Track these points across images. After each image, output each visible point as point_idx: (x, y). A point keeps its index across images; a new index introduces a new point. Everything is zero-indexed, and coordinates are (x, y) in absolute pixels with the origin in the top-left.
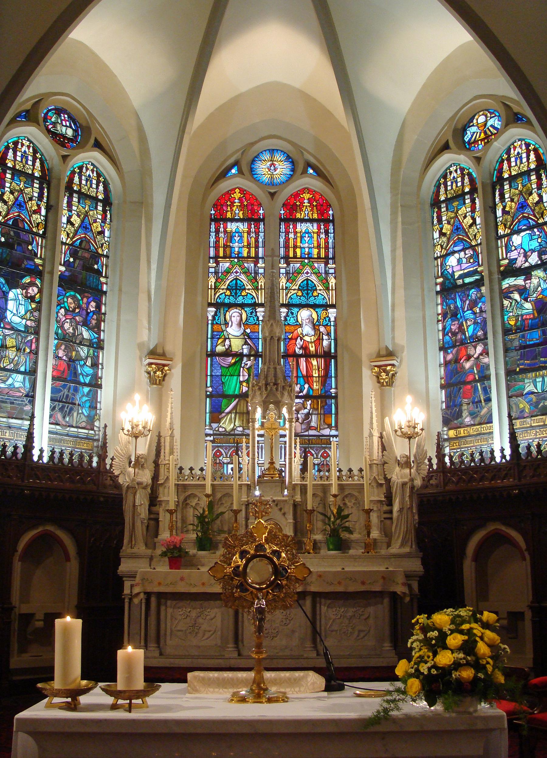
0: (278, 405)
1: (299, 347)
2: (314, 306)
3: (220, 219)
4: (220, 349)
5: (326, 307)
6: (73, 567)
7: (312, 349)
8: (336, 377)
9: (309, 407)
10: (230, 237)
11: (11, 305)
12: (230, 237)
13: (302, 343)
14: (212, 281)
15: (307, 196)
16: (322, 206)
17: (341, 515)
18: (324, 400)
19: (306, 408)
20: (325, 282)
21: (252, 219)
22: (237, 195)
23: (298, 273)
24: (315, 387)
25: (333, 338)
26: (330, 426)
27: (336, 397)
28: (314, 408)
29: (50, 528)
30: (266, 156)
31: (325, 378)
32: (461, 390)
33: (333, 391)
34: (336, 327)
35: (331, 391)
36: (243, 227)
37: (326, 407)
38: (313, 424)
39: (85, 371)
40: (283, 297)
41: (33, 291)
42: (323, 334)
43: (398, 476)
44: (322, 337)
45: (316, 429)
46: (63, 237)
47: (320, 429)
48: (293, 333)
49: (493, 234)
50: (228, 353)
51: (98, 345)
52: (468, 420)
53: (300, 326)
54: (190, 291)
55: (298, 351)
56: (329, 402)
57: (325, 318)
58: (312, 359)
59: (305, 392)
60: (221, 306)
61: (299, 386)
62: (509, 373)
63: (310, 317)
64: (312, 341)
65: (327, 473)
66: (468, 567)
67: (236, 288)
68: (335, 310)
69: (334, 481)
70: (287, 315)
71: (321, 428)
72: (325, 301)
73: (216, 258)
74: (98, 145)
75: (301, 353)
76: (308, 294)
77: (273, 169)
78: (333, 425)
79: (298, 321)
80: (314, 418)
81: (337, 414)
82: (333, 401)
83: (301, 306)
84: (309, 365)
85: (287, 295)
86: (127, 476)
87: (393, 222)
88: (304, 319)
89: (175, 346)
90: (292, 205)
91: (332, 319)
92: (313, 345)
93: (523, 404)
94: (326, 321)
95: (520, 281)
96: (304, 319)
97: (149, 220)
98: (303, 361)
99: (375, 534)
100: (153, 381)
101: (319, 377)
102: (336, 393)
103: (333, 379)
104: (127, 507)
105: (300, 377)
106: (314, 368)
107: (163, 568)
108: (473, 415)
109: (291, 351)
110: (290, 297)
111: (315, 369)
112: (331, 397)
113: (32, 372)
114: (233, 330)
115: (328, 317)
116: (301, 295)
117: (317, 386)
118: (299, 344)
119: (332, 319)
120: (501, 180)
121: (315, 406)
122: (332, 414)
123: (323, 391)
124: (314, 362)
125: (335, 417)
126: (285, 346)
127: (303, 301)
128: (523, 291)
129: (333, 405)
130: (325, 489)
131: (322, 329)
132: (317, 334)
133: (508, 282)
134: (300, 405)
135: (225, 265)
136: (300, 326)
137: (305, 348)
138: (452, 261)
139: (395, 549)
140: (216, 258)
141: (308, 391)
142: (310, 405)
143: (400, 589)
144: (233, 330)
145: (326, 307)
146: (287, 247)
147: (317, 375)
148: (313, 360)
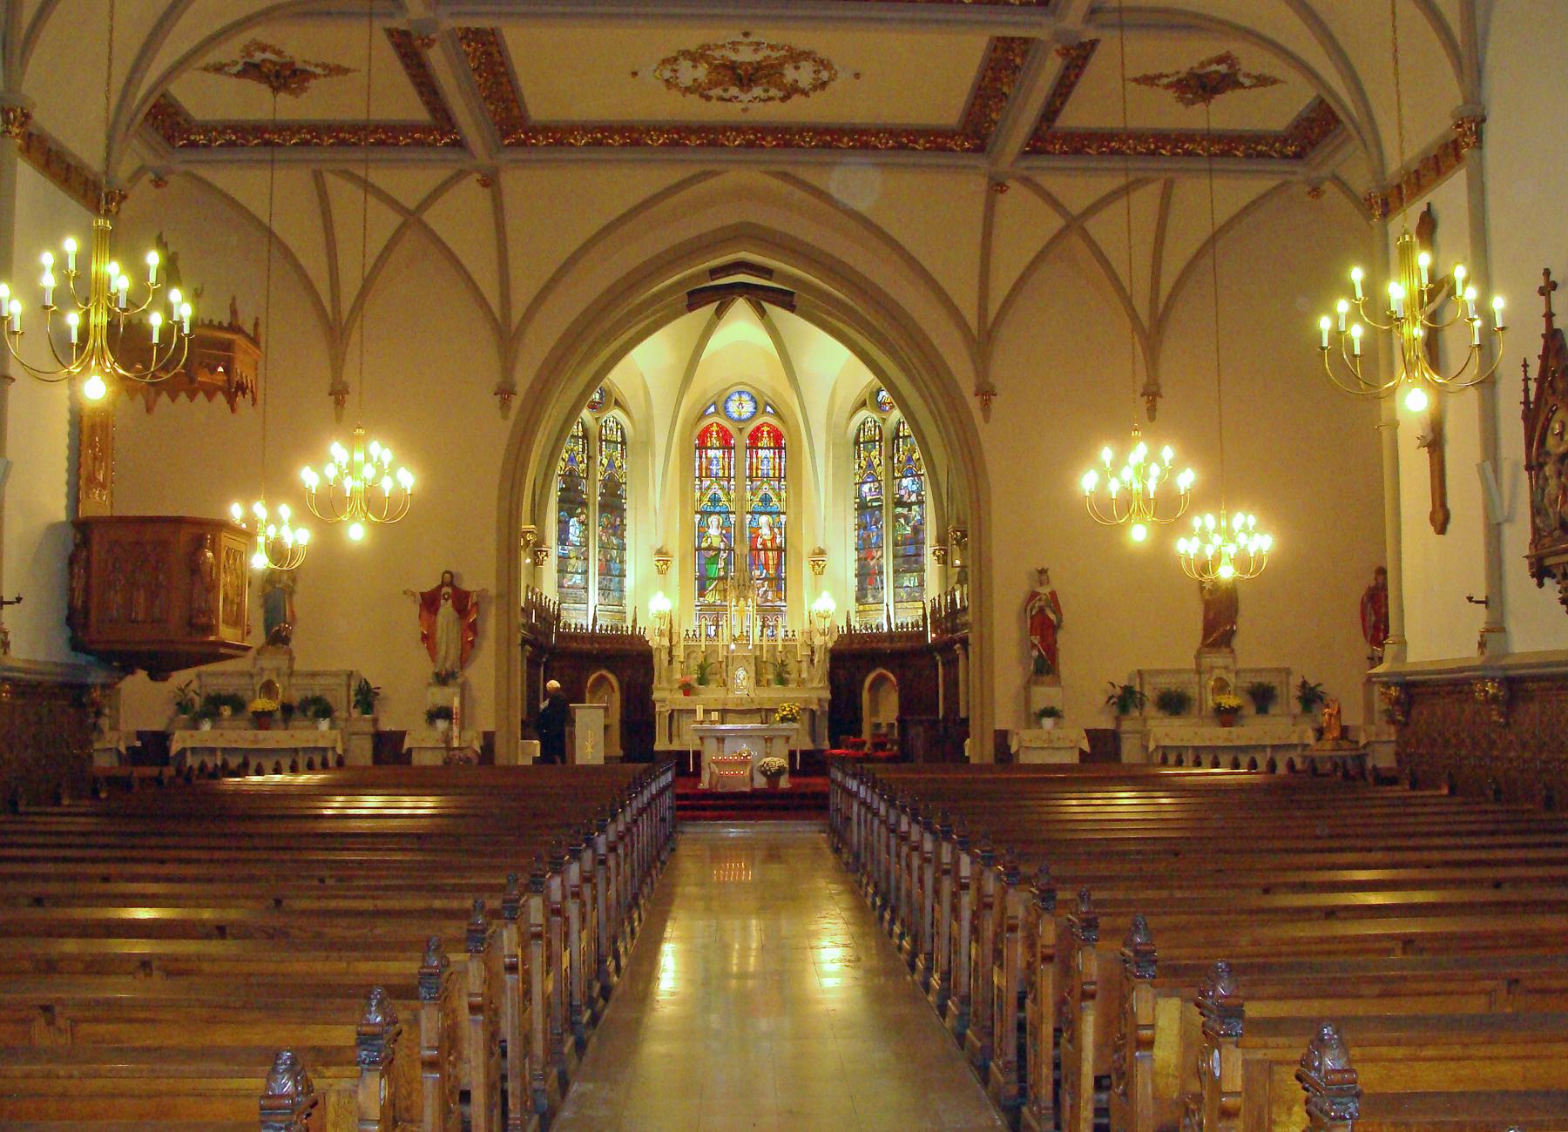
0: (746, 599)
2: (770, 513)
3: (702, 446)
4: (704, 545)
5: (779, 513)
6: (617, 696)
10: (710, 462)
11: (572, 530)
12: (710, 462)
14: (698, 494)
15: (766, 429)
16: (777, 436)
17: (783, 664)
18: (778, 582)
20: (779, 495)
21: (726, 445)
22: (715, 428)
23: (758, 488)
29: (604, 672)
30: (736, 397)
31: (778, 565)
32: (867, 577)
36: (719, 453)
39: (615, 567)
41: (583, 517)
43: (818, 641)
46: (599, 477)
50: (710, 548)
51: (622, 548)
52: (871, 600)
54: (683, 505)
60: (705, 514)
62: (896, 572)
65: (1018, 61)
66: (866, 696)
67: (715, 500)
69: (780, 643)
73: (700, 478)
74: (617, 403)
77: (741, 408)
83: (761, 513)
86: (654, 641)
87: (827, 457)
89: (674, 547)
90: (755, 437)
93: (903, 593)
95: (905, 511)
97: (653, 455)
99: (804, 675)
100: (660, 572)
104: (656, 660)
107: (680, 695)
108: (874, 597)
113: (586, 572)
114: (713, 531)
120: (897, 437)
128: (907, 518)
130: (775, 647)
133: (899, 510)
135: (706, 483)
137: (764, 544)
138: (866, 488)
139: (815, 684)
140: (700, 478)
143: (815, 707)
144: (713, 531)
145: (779, 513)
146: (751, 468)
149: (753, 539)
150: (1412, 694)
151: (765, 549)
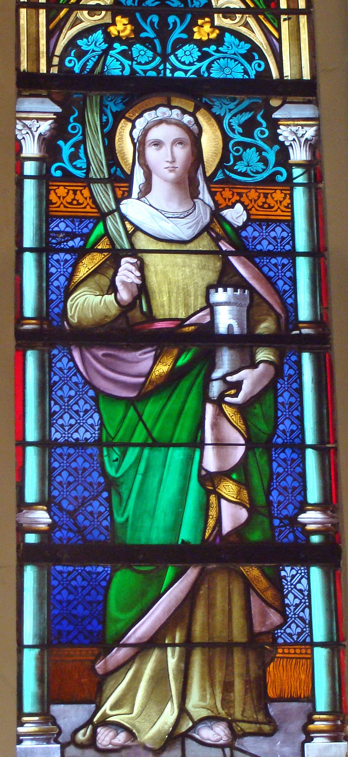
2: (199, 92)
33: (311, 518)
35: (304, 518)
83: (138, 92)
85: (53, 34)
91: (299, 154)
119: (299, 154)
127: (144, 61)
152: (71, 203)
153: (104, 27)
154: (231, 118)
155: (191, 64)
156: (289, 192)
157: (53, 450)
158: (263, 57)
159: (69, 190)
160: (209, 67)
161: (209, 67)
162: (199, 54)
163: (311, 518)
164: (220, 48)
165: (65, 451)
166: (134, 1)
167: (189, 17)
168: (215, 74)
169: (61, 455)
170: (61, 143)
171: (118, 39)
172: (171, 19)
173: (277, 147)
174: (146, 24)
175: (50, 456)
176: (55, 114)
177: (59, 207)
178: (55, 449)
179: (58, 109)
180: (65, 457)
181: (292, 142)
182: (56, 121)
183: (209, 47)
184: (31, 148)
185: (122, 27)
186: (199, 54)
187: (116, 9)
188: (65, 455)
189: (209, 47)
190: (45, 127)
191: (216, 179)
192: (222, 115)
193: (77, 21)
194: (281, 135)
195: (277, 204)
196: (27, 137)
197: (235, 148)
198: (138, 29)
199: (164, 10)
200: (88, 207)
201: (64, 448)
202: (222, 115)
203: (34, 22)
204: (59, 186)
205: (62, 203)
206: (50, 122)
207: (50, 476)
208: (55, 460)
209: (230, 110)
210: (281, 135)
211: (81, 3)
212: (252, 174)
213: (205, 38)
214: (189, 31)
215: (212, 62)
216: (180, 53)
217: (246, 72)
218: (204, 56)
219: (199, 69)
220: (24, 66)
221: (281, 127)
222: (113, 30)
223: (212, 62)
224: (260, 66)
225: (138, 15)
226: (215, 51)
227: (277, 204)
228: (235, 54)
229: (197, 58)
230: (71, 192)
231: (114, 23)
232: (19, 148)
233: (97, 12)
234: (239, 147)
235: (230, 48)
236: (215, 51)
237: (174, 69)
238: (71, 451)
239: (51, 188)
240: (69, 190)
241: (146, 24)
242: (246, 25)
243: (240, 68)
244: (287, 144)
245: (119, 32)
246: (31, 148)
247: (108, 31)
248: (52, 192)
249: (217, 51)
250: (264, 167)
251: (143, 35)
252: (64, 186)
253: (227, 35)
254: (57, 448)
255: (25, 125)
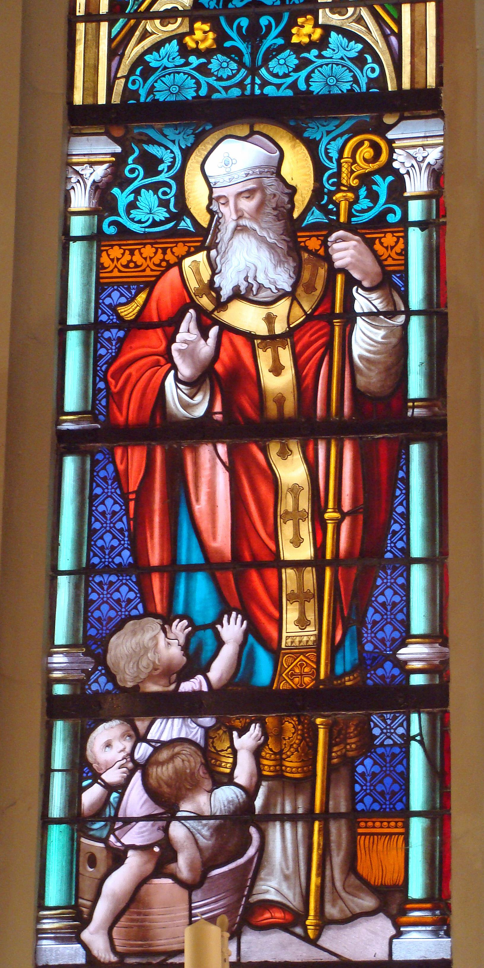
1: (185, 370)
2: (296, 113)
5: (376, 107)
7: (278, 381)
8: (436, 561)
9: (243, 772)
13: (206, 348)
19: (229, 779)
24: (294, 627)
25: (416, 298)
26: (391, 901)
27: (434, 699)
28: (279, 776)
31: (362, 570)
33: (414, 653)
34: (441, 228)
35: (404, 653)
37: (367, 766)
38: (273, 887)
40: (92, 69)
42: (351, 282)
44: (349, 300)
45: (291, 921)
47: (325, 922)
48: (151, 286)
49: (120, 284)
53: (203, 238)
55: (183, 402)
56: (388, 733)
57: (366, 179)
58: (274, 449)
59: (219, 670)
61: (179, 628)
63: (270, 181)
64: (280, 328)
68: (435, 127)
70: (117, 177)
71: (332, 911)
72: (370, 71)
75: (200, 412)
76: (254, 36)
78: (416, 889)
79: (183, 210)
80: (281, 842)
81: (439, 816)
82: (416, 723)
83: (206, 117)
84: (251, 483)
85: (116, 51)
88: (230, 192)
91: (417, 184)
92: (285, 356)
94: (373, 197)
96: (230, 192)
98: (211, 474)
101: (318, 562)
102: (438, 669)
103: (418, 576)
105: (191, 569)
106: (287, 503)
109: (130, 412)
110: (140, 60)
111: (296, 516)
112: (401, 698)
115: (388, 169)
116: (209, 42)
117: (302, 622)
118: (189, 354)
119: (417, 184)
121: (292, 765)
122: (407, 814)
123: (348, 658)
124: (292, 470)
125: (430, 833)
126: (97, 369)
127: (225, 78)
129: (417, 754)
131: (346, 251)
132: (310, 288)
134: (187, 760)
136: (203, 238)
137: (228, 377)
141: (244, 660)
142: (257, 753)
145: (376, 107)
147: (306, 552)
148: (284, 453)
149: (126, 337)
150: (212, 835)
151: (245, 424)
152: (126, 266)
153: (180, 38)
154: (328, 143)
155: (286, 76)
156: (402, 234)
157: (91, 579)
158: (377, 59)
159: (157, 249)
160: (308, 78)
161: (308, 78)
162: (296, 62)
163: (414, 653)
164: (324, 53)
165: (106, 580)
166: (218, 3)
167: (286, 16)
168: (316, 88)
169: (100, 584)
170: (116, 191)
171: (197, 52)
172: (264, 21)
173: (390, 178)
174: (233, 31)
175: (87, 586)
176: (113, 155)
177: (112, 271)
178: (93, 578)
179: (118, 149)
180: (105, 587)
181: (409, 169)
182: (113, 165)
183: (309, 52)
184: (80, 200)
185: (202, 35)
186: (296, 62)
187: (196, 13)
188: (106, 584)
189: (309, 52)
190: (99, 172)
191: (305, 223)
192: (318, 139)
193: (145, 35)
194: (397, 160)
195: (387, 250)
196: (77, 187)
197: (330, 182)
198: (221, 37)
199: (255, 8)
200: (148, 269)
201: (104, 575)
202: (318, 139)
203: (93, 43)
204: (177, 243)
205: (116, 267)
206: (106, 166)
207: (86, 611)
208: (94, 591)
209: (328, 133)
210: (397, 160)
211: (151, 11)
212: (358, 214)
213: (306, 40)
214: (286, 34)
215: (313, 71)
216: (272, 64)
217: (355, 80)
218: (304, 63)
219: (295, 82)
220: (78, 99)
221: (396, 150)
222: (189, 42)
223: (313, 71)
224: (373, 70)
225: (222, 20)
226: (316, 57)
227: (387, 250)
228: (342, 58)
229: (294, 67)
230: (160, 251)
231: (191, 32)
232: (67, 200)
233: (172, 21)
234: (140, 168)
235: (337, 51)
236: (316, 57)
237: (265, 83)
238: (113, 578)
239: (103, 248)
240: (125, 250)
241: (233, 31)
242: (360, 20)
243: (348, 76)
244: (403, 171)
245: (197, 43)
246: (80, 200)
247: (184, 42)
248: (104, 254)
249: (320, 56)
250: (371, 205)
251: (227, 44)
252: (184, 242)
253: (333, 34)
254: (95, 576)
255: (77, 173)
